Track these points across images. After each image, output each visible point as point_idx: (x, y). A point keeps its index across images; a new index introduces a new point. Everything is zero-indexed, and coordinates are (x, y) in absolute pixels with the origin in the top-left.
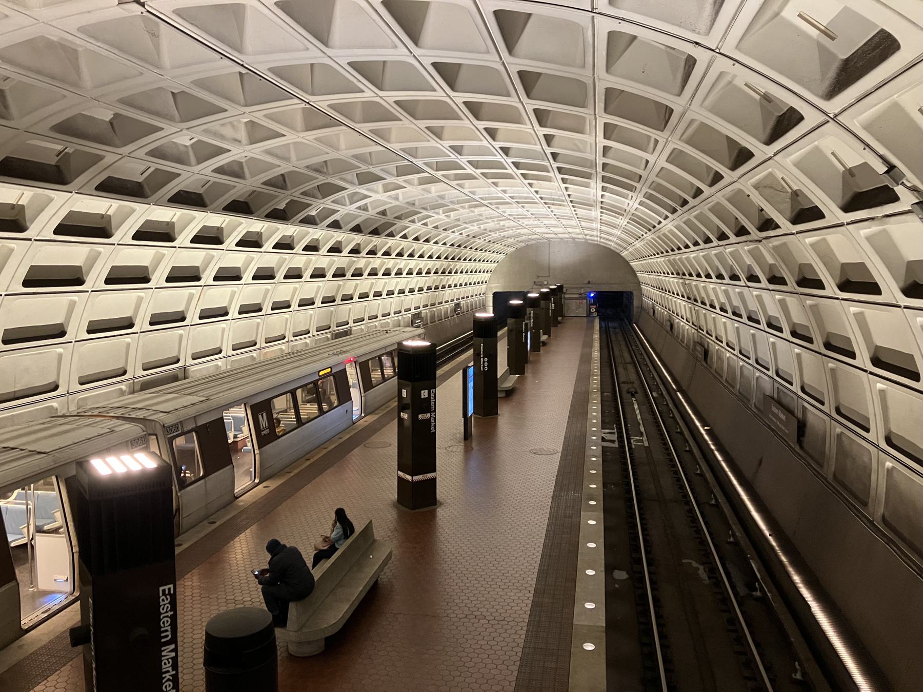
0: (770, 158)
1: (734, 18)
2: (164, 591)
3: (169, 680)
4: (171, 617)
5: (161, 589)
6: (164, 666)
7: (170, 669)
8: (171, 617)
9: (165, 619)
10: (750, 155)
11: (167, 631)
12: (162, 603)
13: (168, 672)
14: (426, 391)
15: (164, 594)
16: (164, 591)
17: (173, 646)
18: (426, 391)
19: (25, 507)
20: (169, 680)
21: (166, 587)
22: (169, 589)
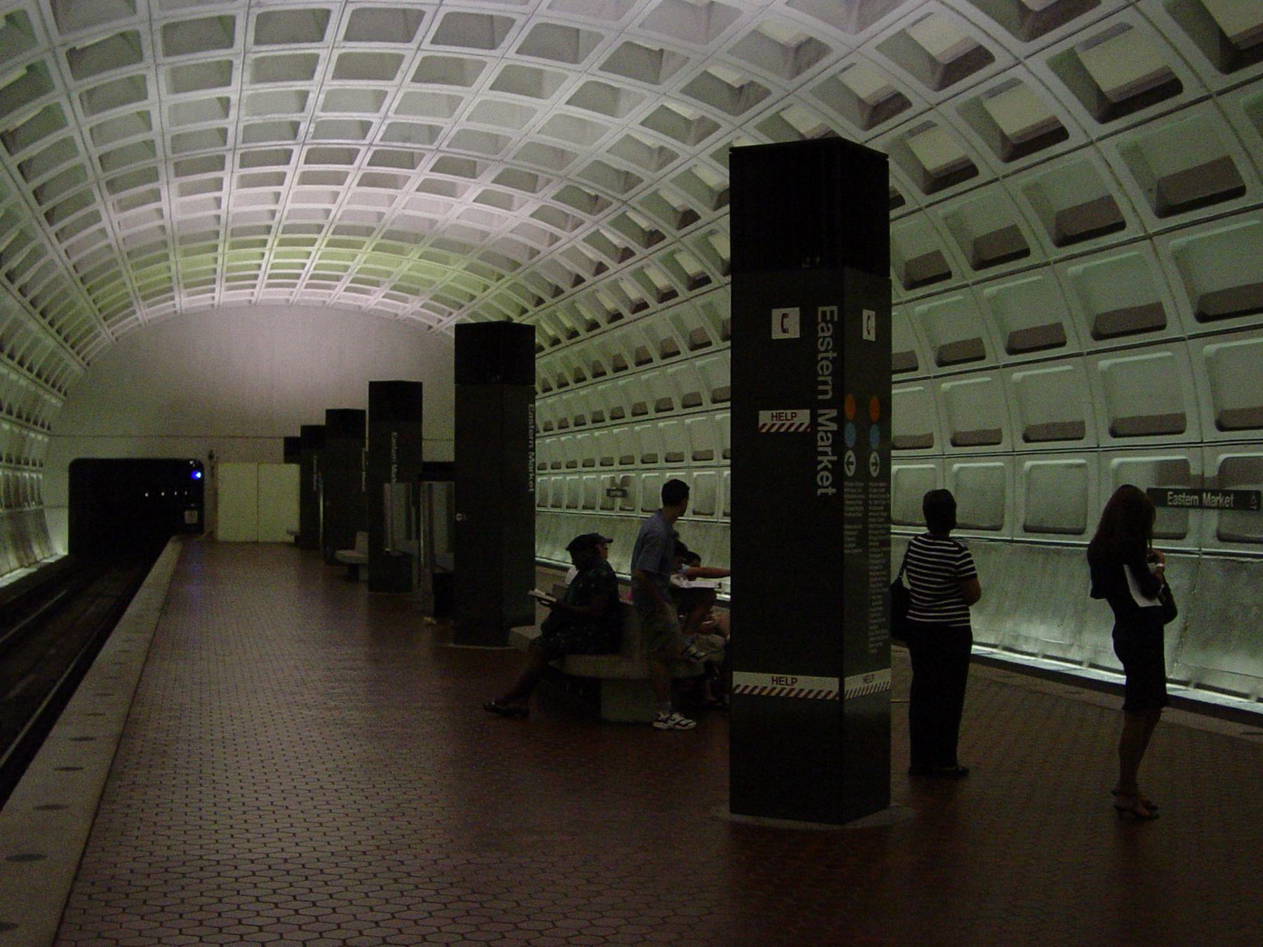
0: (1183, 339)
1: (43, 20)
2: (824, 313)
3: (825, 468)
4: (833, 361)
5: (821, 309)
6: (820, 443)
7: (829, 450)
8: (833, 361)
9: (825, 363)
10: (562, 292)
11: (825, 383)
12: (820, 334)
13: (825, 454)
14: (794, 313)
15: (824, 320)
16: (824, 313)
17: (834, 413)
18: (794, 313)
19: (440, 490)
20: (825, 468)
21: (827, 309)
22: (832, 313)
